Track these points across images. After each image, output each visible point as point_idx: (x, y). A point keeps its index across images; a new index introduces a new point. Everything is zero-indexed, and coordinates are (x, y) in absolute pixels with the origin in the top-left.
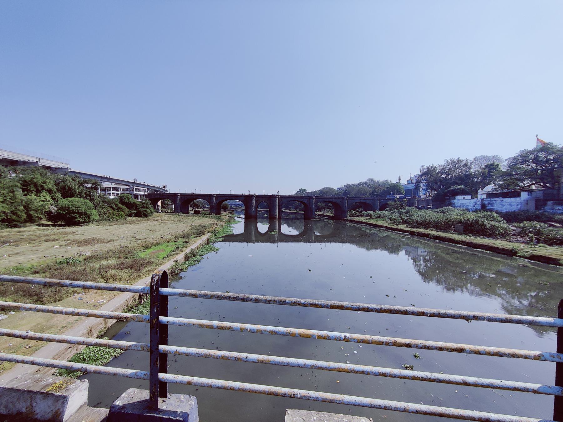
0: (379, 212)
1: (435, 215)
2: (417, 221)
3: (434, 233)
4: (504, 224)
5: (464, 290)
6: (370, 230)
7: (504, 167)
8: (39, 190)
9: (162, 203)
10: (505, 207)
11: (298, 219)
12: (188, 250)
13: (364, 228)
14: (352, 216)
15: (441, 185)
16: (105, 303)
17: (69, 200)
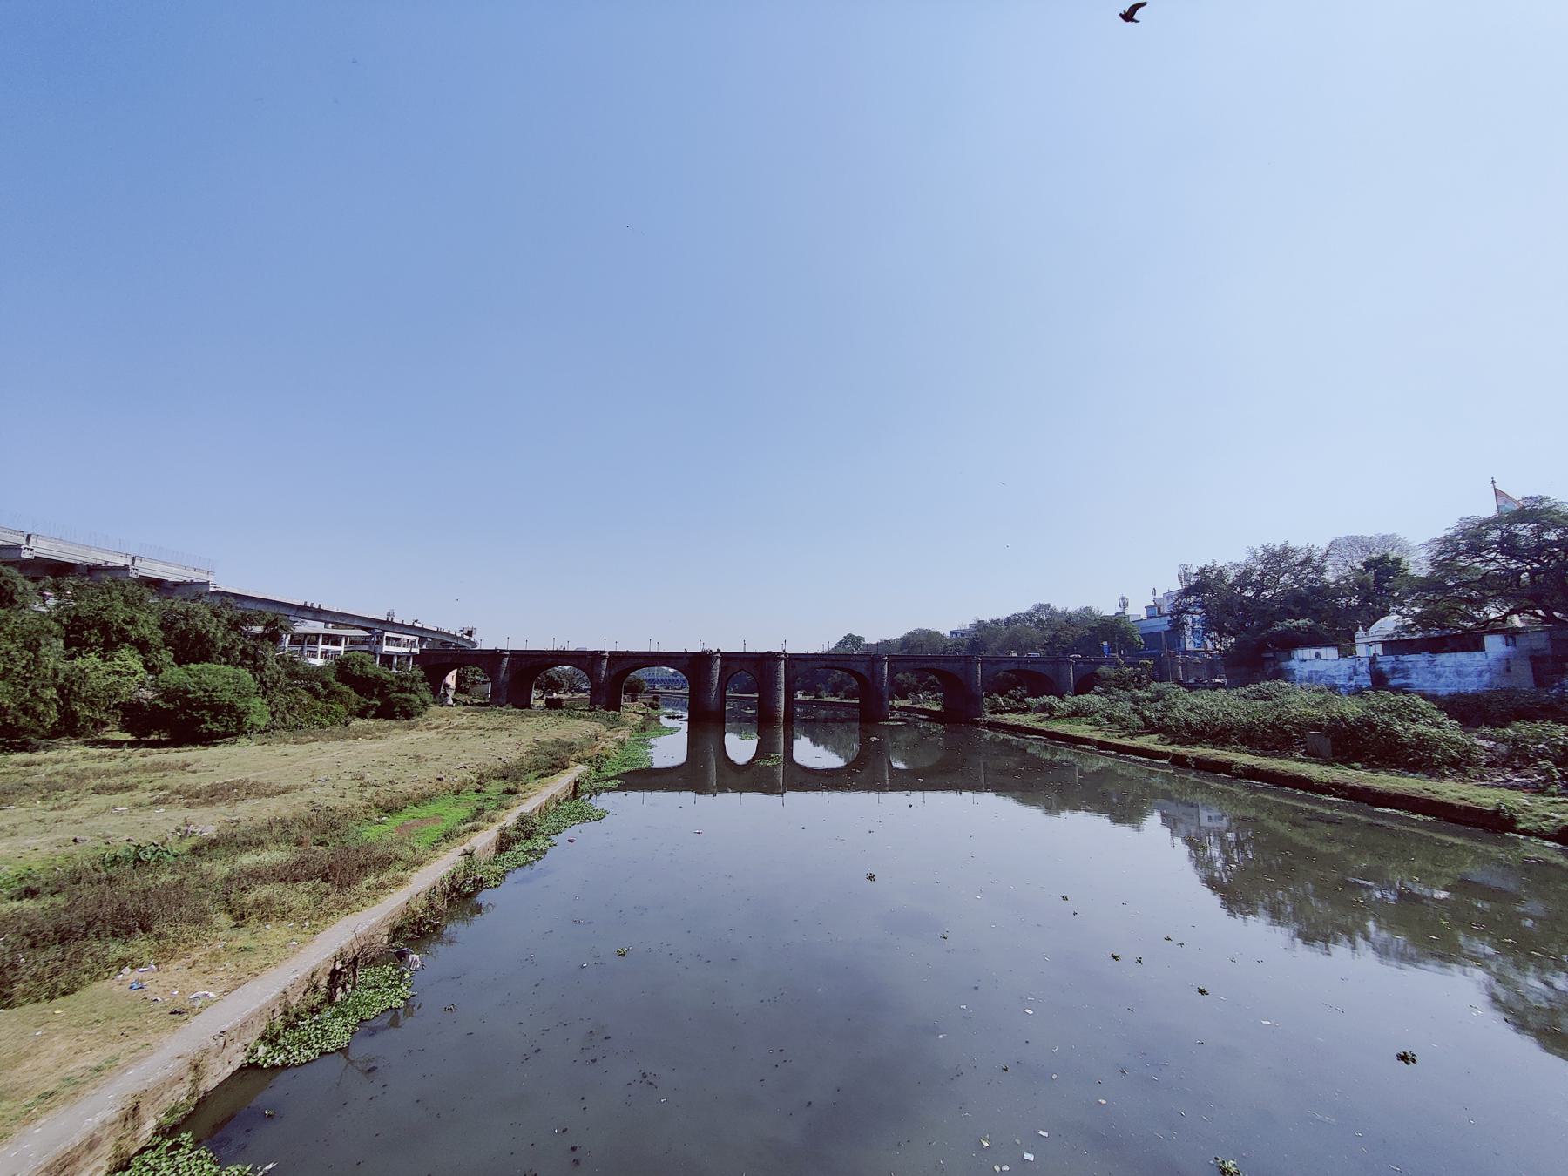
0: (1075, 699)
1: (1242, 704)
2: (1188, 724)
3: (1245, 759)
4: (1452, 730)
5: (1360, 941)
6: (1054, 753)
7: (1419, 565)
8: (111, 639)
9: (459, 679)
10: (1442, 680)
11: (842, 721)
12: (510, 818)
13: (1035, 747)
14: (996, 710)
15: (1245, 618)
16: (213, 1001)
17: (190, 666)
